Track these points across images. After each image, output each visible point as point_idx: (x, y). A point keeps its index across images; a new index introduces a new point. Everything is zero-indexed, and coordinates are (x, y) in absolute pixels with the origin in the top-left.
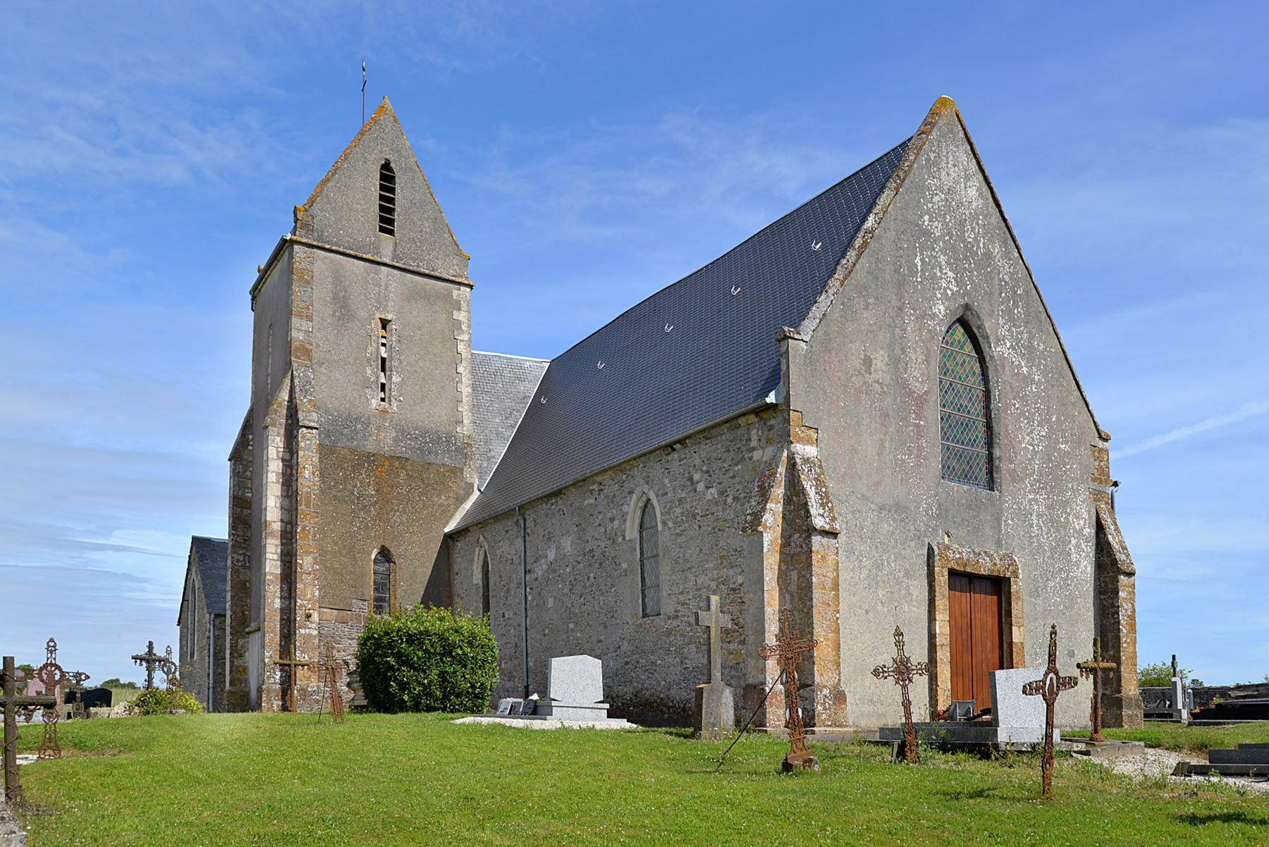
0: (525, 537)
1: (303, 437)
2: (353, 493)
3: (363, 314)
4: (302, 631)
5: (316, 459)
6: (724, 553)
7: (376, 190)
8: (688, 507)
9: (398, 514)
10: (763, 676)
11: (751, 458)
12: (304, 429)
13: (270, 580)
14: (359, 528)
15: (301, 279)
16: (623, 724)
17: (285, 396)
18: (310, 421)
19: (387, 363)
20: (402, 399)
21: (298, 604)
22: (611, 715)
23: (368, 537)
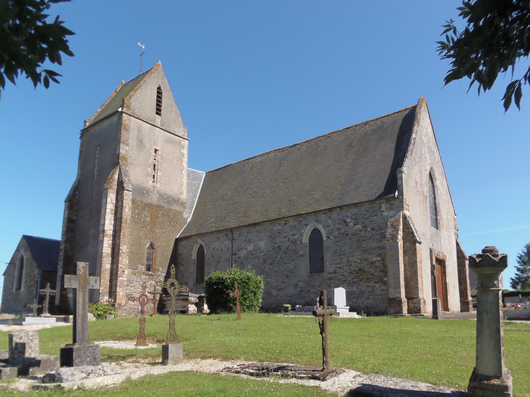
0: (232, 240)
1: (126, 194)
2: (141, 220)
3: (147, 145)
4: (120, 278)
5: (130, 205)
6: (365, 249)
7: (155, 97)
8: (343, 231)
9: (158, 229)
10: (399, 295)
11: (382, 215)
12: (126, 191)
13: (104, 256)
14: (143, 234)
15: (125, 129)
16: (354, 315)
17: (116, 176)
18: (129, 188)
19: (156, 167)
20: (161, 182)
21: (119, 267)
22: (351, 310)
23: (146, 238)
